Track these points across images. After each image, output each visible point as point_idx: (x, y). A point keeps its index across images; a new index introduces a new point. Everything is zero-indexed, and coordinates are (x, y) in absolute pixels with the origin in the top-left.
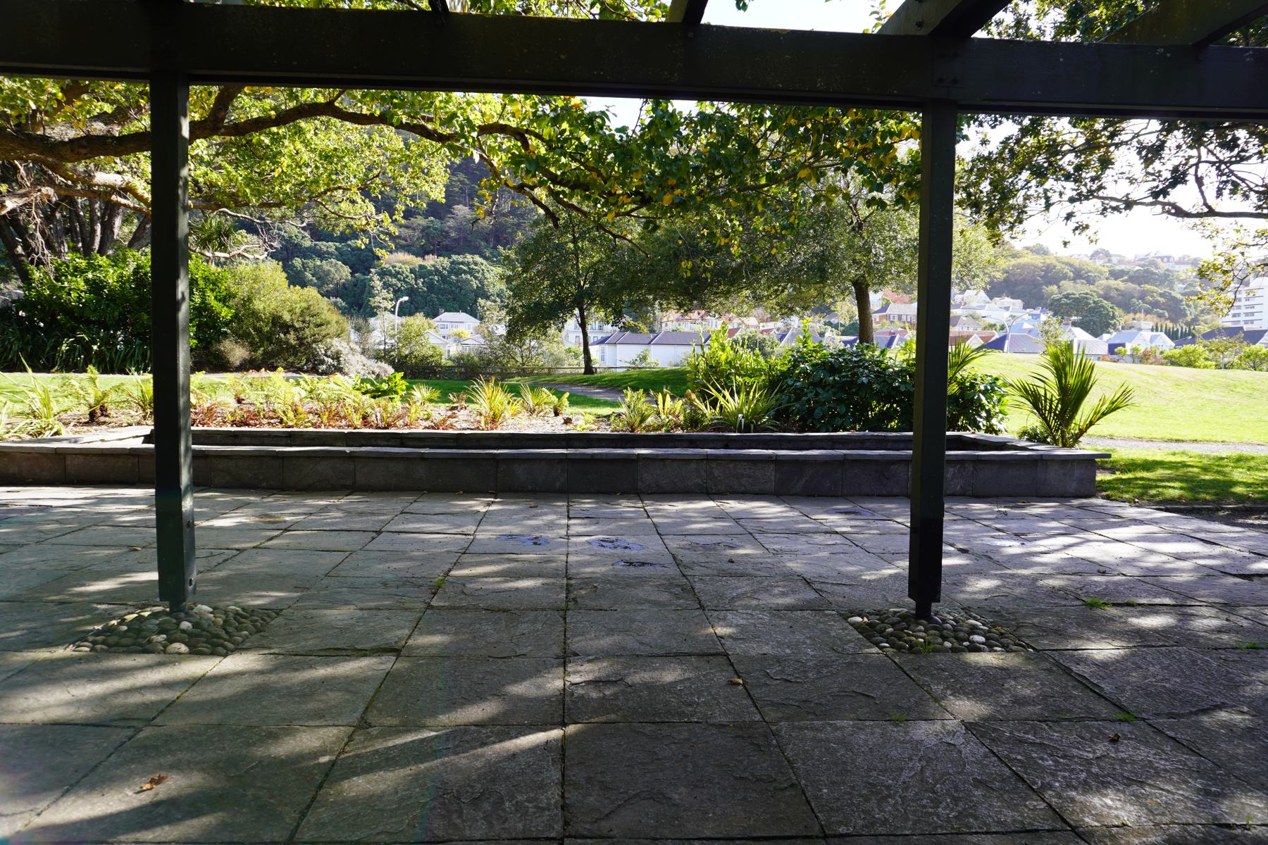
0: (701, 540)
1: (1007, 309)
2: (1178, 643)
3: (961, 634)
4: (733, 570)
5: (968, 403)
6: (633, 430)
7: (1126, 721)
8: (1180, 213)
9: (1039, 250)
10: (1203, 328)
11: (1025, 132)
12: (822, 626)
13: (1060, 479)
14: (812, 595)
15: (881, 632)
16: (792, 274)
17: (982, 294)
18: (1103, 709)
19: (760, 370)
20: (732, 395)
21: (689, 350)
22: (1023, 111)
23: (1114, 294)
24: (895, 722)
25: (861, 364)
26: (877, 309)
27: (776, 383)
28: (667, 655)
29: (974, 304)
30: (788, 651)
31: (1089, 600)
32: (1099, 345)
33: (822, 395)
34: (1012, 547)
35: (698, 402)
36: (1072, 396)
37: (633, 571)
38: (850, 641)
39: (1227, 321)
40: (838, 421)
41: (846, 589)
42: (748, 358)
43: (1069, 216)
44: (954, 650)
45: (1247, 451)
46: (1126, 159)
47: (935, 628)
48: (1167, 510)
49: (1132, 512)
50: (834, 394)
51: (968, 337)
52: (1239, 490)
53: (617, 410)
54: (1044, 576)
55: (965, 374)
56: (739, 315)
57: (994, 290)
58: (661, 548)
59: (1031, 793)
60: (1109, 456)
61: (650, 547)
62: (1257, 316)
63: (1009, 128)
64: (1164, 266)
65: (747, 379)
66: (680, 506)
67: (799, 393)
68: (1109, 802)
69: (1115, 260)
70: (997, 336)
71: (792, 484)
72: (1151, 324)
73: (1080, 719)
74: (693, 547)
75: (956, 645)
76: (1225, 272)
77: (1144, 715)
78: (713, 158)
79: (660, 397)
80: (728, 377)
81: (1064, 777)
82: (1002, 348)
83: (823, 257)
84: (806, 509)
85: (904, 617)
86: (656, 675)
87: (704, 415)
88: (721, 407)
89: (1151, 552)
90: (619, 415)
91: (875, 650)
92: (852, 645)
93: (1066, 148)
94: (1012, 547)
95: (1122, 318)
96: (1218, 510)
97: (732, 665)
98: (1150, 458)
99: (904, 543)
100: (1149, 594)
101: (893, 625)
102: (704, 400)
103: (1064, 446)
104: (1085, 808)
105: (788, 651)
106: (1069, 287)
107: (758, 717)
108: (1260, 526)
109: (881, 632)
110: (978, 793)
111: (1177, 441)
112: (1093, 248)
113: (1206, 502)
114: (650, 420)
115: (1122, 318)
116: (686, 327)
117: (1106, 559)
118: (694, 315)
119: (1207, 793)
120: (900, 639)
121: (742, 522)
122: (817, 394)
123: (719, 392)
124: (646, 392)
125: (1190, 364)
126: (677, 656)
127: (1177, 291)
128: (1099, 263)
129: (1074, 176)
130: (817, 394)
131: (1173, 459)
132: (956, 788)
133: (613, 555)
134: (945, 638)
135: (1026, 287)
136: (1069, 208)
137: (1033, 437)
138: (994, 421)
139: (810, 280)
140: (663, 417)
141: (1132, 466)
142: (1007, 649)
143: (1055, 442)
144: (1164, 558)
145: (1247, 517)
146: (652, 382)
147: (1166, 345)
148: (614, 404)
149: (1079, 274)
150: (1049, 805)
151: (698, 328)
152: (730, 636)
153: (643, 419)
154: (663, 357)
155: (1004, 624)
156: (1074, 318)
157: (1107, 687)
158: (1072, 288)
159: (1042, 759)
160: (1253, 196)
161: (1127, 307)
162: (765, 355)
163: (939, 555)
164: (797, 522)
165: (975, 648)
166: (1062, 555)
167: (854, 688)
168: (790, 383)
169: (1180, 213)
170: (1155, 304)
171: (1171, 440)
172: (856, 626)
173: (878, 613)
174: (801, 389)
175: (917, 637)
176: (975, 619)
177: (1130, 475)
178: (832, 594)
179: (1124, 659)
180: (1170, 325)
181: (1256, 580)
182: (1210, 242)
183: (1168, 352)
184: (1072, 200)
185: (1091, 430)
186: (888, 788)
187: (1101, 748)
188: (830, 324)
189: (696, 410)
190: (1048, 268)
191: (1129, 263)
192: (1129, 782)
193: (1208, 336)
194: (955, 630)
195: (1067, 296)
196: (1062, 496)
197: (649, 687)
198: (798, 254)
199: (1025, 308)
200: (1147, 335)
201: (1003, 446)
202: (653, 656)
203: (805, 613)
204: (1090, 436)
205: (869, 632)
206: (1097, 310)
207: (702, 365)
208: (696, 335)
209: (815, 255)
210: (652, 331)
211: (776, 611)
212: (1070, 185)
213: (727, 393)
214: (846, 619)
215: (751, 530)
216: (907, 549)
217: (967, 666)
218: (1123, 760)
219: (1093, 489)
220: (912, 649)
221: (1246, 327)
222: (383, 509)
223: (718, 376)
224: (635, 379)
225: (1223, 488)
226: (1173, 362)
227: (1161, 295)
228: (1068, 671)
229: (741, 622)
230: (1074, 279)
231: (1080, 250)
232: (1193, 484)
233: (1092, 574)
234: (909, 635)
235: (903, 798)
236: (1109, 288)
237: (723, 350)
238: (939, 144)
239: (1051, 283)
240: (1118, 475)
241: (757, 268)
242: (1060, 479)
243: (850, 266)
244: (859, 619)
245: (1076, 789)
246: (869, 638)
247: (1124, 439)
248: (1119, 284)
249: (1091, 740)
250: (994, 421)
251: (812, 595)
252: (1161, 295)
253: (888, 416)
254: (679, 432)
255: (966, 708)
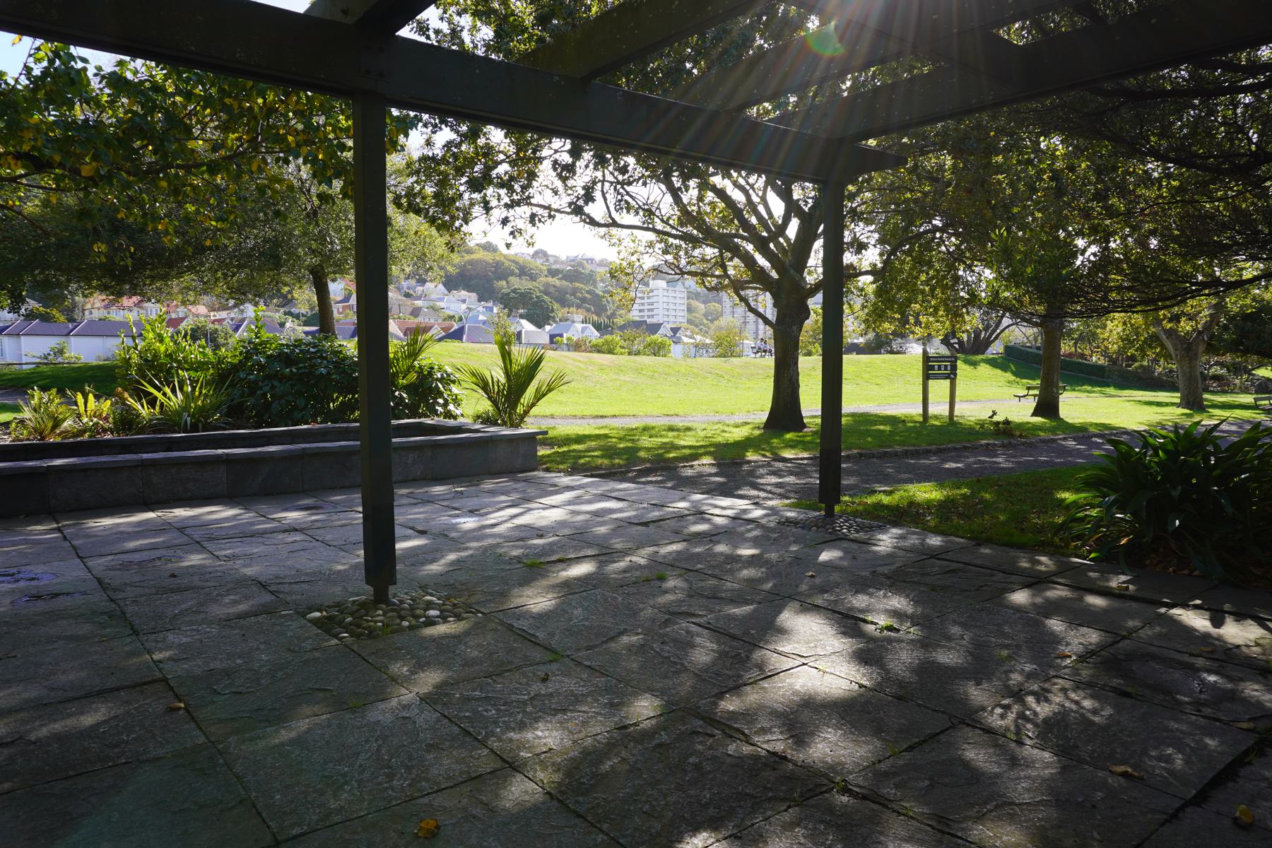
0: (137, 557)
1: (464, 301)
2: (595, 587)
3: (418, 612)
4: (179, 584)
5: (427, 388)
6: (43, 438)
7: (555, 661)
8: (593, 222)
9: (488, 247)
10: (619, 321)
11: (465, 137)
12: (279, 628)
13: (507, 457)
14: (267, 598)
15: (340, 623)
16: (243, 259)
17: (441, 286)
18: (537, 654)
19: (207, 363)
20: (174, 391)
21: (117, 341)
22: (460, 116)
23: (552, 290)
24: (352, 710)
25: (320, 354)
26: (339, 298)
27: (225, 376)
28: (86, 696)
29: (434, 296)
30: (239, 661)
31: (529, 562)
32: (542, 336)
33: (264, 388)
34: (469, 523)
35: (131, 401)
36: (520, 379)
37: (41, 606)
38: (308, 638)
39: (635, 315)
40: (297, 415)
41: (305, 586)
42: (195, 352)
43: (505, 221)
44: (411, 628)
45: (651, 422)
46: (546, 172)
47: (393, 611)
48: (592, 476)
49: (566, 480)
50: (292, 386)
51: (431, 328)
52: (642, 454)
53: (19, 416)
54: (498, 545)
55: (424, 363)
56: (183, 303)
57: (451, 284)
58: (83, 573)
59: (476, 743)
60: (546, 433)
61: (69, 572)
62: (655, 312)
63: (445, 135)
64: (589, 267)
65: (192, 374)
66: (107, 522)
67: (253, 387)
68: (540, 733)
69: (551, 260)
70: (456, 327)
71: (243, 484)
72: (581, 317)
73: (518, 668)
74: (125, 566)
75: (413, 622)
76: (627, 274)
77: (569, 653)
78: (135, 128)
79: (80, 398)
80: (169, 371)
81: (504, 722)
82: (461, 339)
83: (276, 243)
84: (263, 508)
85: (363, 605)
86: (70, 722)
87: (139, 415)
88: (162, 404)
89: (579, 513)
90: (22, 422)
91: (335, 641)
92: (310, 641)
93: (502, 157)
94: (469, 523)
95: (561, 312)
96: (628, 472)
97: (172, 689)
98: (581, 433)
99: (359, 534)
100: (576, 549)
101: (352, 615)
102: (140, 400)
103: (512, 426)
104: (522, 745)
105: (239, 661)
106: (516, 282)
107: (202, 739)
108: (656, 482)
109: (340, 623)
110: (430, 757)
111: (602, 417)
112: (531, 251)
113: (620, 466)
114: (67, 424)
115: (561, 312)
116: (116, 315)
117: (543, 523)
118: (126, 301)
119: (612, 705)
120: (359, 626)
121: (188, 531)
122: (273, 387)
123: (159, 389)
124: (61, 392)
125: (611, 352)
126: (99, 694)
127: (600, 288)
128: (539, 262)
129: (507, 184)
130: (273, 387)
131: (597, 432)
132: (410, 758)
133: (13, 591)
134: (403, 618)
135: (481, 279)
136: (504, 213)
137: (487, 420)
138: (451, 407)
139: (258, 270)
140: (85, 420)
141: (568, 440)
142: (459, 618)
143: (504, 423)
144: (588, 516)
145: (648, 475)
146: (67, 380)
147: (593, 334)
148: (16, 409)
149: (524, 271)
150: (492, 750)
151: (131, 317)
152: (170, 659)
153: (57, 423)
154: (84, 350)
155: (460, 593)
156: (521, 311)
157: (541, 635)
158: (519, 284)
159: (487, 711)
160: (641, 213)
161: (563, 303)
162: (217, 347)
163: (392, 540)
164: (252, 524)
165: (431, 623)
166: (509, 525)
167: (310, 685)
168: (242, 375)
169: (593, 222)
170: (584, 300)
171: (597, 417)
172: (315, 622)
173: (337, 605)
174: (256, 382)
175: (376, 622)
176: (431, 595)
177: (565, 449)
178: (290, 593)
179: (557, 607)
180: (596, 318)
181: (651, 526)
182: (616, 249)
183: (594, 342)
184: (507, 206)
185: (534, 411)
186: (344, 775)
187: (537, 687)
188: (290, 314)
189: (130, 409)
190: (498, 265)
191: (562, 263)
192: (556, 712)
193: (622, 328)
194: (412, 609)
195: (514, 291)
196: (509, 471)
197: (58, 738)
198: (247, 237)
199: (480, 301)
200: (579, 326)
201: (459, 429)
202: (68, 701)
203: (260, 618)
204: (536, 416)
205: (327, 625)
206: (539, 304)
207: (135, 359)
208: (124, 325)
209: (266, 241)
210: (71, 320)
211: (227, 622)
212: (503, 192)
213: (167, 390)
214: (304, 615)
215: (193, 536)
216: (361, 537)
217: (424, 639)
218: (551, 695)
219: (533, 463)
220: (372, 634)
221: (649, 321)
222: (1008, 549)
223: (158, 369)
224: (48, 377)
225: (631, 454)
226: (598, 349)
227: (588, 292)
228: (510, 628)
229: (185, 640)
230: (520, 276)
231: (520, 249)
232: (610, 452)
233: (532, 538)
234: (368, 621)
235: (359, 782)
236: (547, 285)
237: (161, 341)
238: (376, 143)
239: (500, 279)
240: (556, 449)
241: (201, 250)
242: (507, 457)
243: (306, 254)
244: (317, 614)
245: (514, 730)
246: (328, 631)
247: (565, 417)
248: (555, 281)
249: (527, 684)
250: (451, 407)
251: (267, 598)
252: (588, 292)
253: (346, 408)
254: (108, 436)
255: (430, 679)
